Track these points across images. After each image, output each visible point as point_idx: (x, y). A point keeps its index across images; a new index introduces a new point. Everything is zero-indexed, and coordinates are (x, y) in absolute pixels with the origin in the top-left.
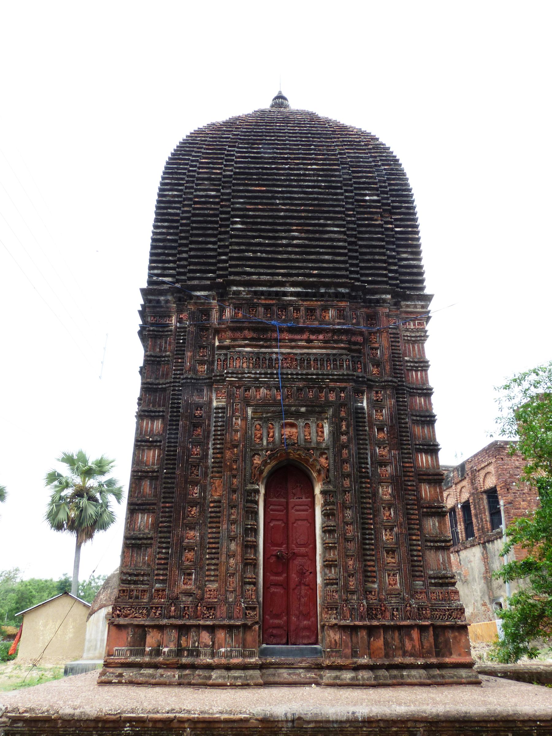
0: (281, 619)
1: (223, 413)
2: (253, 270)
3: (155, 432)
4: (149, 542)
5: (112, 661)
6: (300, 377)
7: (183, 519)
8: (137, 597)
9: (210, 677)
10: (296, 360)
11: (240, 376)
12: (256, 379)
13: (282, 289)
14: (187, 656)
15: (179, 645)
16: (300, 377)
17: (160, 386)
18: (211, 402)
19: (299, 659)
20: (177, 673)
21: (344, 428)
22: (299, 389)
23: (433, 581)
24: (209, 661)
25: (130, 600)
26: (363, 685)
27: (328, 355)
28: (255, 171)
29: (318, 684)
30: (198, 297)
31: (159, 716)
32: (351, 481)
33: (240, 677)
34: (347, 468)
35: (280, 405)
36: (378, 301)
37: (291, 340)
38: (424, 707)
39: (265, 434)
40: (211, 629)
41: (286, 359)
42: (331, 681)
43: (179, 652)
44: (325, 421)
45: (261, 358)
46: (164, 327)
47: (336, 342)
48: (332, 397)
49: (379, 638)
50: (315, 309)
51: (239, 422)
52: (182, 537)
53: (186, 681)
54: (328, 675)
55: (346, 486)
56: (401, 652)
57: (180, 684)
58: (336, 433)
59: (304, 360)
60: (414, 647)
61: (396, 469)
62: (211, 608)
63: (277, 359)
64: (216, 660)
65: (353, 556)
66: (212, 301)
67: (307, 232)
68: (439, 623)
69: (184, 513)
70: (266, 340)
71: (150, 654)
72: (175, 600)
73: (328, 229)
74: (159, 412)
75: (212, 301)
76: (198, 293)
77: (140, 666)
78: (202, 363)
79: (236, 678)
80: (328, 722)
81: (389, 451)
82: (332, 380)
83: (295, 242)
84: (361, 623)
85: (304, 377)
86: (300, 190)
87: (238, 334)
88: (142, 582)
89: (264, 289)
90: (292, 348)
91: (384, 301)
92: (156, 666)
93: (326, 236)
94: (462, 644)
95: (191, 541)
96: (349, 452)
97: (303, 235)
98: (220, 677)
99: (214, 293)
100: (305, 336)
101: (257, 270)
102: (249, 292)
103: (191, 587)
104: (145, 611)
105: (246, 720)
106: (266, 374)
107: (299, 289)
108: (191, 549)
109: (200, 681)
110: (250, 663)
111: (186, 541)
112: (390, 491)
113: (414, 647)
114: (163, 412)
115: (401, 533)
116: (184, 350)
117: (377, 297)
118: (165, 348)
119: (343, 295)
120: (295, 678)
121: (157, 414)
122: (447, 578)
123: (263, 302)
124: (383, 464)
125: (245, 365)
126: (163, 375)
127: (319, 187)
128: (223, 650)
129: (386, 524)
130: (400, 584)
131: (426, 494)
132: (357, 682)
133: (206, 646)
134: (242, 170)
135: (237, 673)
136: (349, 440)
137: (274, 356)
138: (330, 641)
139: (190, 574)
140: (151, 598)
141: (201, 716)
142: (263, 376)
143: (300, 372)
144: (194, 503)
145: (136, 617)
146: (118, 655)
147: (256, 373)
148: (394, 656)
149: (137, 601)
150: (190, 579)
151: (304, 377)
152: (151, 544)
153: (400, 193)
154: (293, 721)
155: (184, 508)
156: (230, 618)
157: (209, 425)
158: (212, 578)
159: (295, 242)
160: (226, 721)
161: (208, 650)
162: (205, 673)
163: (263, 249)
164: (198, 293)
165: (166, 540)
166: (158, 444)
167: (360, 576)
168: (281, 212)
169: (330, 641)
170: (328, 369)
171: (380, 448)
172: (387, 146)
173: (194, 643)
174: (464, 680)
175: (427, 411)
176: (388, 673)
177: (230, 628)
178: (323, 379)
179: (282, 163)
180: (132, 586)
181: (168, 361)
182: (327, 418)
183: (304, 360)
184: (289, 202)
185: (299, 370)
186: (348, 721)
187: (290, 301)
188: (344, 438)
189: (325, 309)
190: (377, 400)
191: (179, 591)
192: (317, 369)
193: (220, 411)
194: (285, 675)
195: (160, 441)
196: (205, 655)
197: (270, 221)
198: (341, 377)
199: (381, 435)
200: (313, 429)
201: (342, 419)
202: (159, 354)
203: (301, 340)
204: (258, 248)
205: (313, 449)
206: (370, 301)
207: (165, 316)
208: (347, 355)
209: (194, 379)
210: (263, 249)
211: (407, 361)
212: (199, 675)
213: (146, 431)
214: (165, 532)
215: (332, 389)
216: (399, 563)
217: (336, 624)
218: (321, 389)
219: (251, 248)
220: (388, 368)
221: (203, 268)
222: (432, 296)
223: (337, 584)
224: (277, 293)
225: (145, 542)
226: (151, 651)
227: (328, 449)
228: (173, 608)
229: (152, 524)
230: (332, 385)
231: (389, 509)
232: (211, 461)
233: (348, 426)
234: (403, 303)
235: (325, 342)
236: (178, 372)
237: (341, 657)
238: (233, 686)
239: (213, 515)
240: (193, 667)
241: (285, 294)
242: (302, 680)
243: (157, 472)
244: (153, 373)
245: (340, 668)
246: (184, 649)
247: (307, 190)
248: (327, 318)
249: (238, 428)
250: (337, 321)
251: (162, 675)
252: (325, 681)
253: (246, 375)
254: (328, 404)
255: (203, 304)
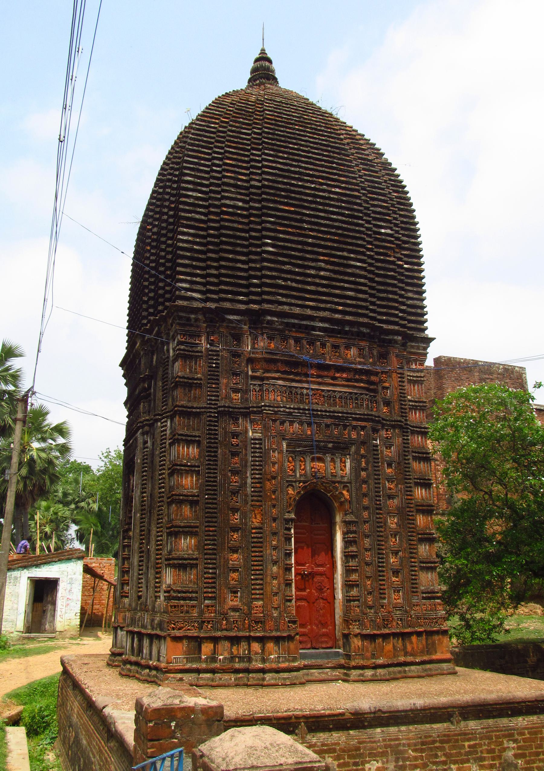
0: (306, 628)
1: (260, 444)
2: (284, 300)
3: (192, 456)
4: (195, 562)
5: (172, 668)
6: (328, 414)
7: (228, 543)
8: (187, 612)
9: (264, 679)
10: (324, 396)
11: (276, 409)
12: (290, 414)
13: (312, 323)
14: (239, 662)
15: (232, 653)
16: (328, 414)
17: (194, 410)
18: (246, 431)
19: (326, 661)
20: (233, 677)
21: (363, 464)
22: (327, 426)
23: (424, 595)
24: (261, 666)
25: (182, 615)
26: (381, 680)
27: (351, 393)
28: (283, 187)
29: (344, 681)
30: (231, 321)
31: (279, 714)
32: (369, 513)
33: (288, 678)
34: (366, 502)
35: (312, 440)
36: (390, 341)
37: (318, 376)
38: (457, 697)
39: (298, 467)
40: (261, 640)
41: (315, 395)
42: (357, 678)
43: (232, 659)
44: (348, 457)
45: (294, 392)
46: (192, 347)
47: (357, 381)
48: (354, 435)
49: (389, 643)
50: (338, 346)
51: (276, 454)
52: (228, 559)
53: (242, 683)
54: (355, 673)
55: (365, 517)
56: (403, 653)
57: (237, 685)
58: (357, 469)
59: (330, 397)
60: (413, 648)
61: (402, 501)
62: (258, 622)
63: (307, 395)
64: (267, 665)
65: (371, 577)
66: (243, 326)
67: (332, 264)
68: (429, 629)
69: (228, 538)
70: (297, 374)
71: (206, 661)
72: (225, 615)
73: (353, 263)
74: (195, 436)
75: (243, 326)
76: (231, 317)
77: (198, 671)
78: (236, 391)
79: (285, 679)
80: (398, 711)
81: (396, 486)
82: (355, 419)
83: (322, 273)
84: (378, 632)
85: (331, 414)
86: (326, 215)
87: (272, 367)
88: (191, 599)
89: (296, 321)
90: (319, 384)
91: (396, 342)
92: (213, 671)
93: (349, 271)
94: (444, 644)
95: (235, 563)
96: (368, 487)
97: (329, 267)
98: (273, 678)
99: (246, 318)
100: (331, 373)
101: (289, 300)
102: (282, 323)
103: (237, 603)
104: (196, 625)
105: (342, 714)
106: (299, 409)
107: (326, 325)
108: (235, 570)
109: (255, 682)
110: (295, 667)
111: (231, 562)
112: (396, 520)
113: (413, 648)
114: (199, 437)
115: (405, 557)
116: (218, 376)
117: (390, 337)
118: (195, 369)
119: (364, 335)
120: (324, 676)
121: (193, 439)
122: (434, 592)
123: (294, 334)
124: (391, 497)
125: (279, 398)
126: (195, 397)
127: (343, 215)
128: (272, 657)
129: (393, 549)
130: (403, 599)
131: (420, 522)
132: (376, 678)
133: (256, 653)
134: (271, 184)
135: (286, 675)
136: (368, 476)
137: (305, 391)
138: (355, 647)
139: (236, 592)
140: (201, 613)
141: (312, 713)
142: (296, 411)
143: (328, 410)
144: (235, 529)
145: (189, 630)
146: (177, 662)
147: (290, 408)
148: (398, 656)
149: (188, 615)
150: (235, 597)
151: (331, 414)
152: (197, 564)
153: (408, 226)
154: (374, 713)
155: (228, 533)
156: (277, 630)
157: (246, 455)
158: (258, 596)
159: (322, 273)
160: (330, 716)
161: (259, 657)
162: (260, 675)
163: (294, 277)
164: (231, 317)
165: (212, 561)
166: (197, 469)
167: (376, 593)
168: (309, 238)
169: (355, 647)
170: (351, 408)
171: (388, 482)
172: (393, 166)
173: (244, 651)
174: (445, 672)
175: (423, 447)
176: (396, 670)
177: (277, 640)
178: (348, 417)
179: (308, 181)
180: (182, 602)
181: (201, 384)
182: (349, 454)
183: (330, 397)
184: (317, 228)
185: (326, 407)
186: (411, 710)
187: (318, 335)
188: (363, 474)
189: (348, 348)
190: (387, 438)
191: (229, 607)
192: (342, 407)
193: (257, 442)
194: (316, 674)
195: (198, 467)
196: (256, 661)
197: (300, 247)
198: (362, 417)
199: (389, 471)
200: (338, 464)
201: (363, 456)
202: (191, 376)
203: (327, 377)
204: (289, 276)
205: (339, 482)
206: (384, 341)
207: (195, 335)
208: (367, 395)
209: (231, 408)
210: (294, 277)
211: (410, 401)
212: (253, 678)
213: (183, 455)
214: (210, 554)
215: (354, 428)
216: (403, 582)
217: (359, 633)
218: (345, 427)
219: (283, 275)
220: (397, 407)
221: (235, 289)
222: (433, 339)
223: (358, 600)
224: (307, 327)
225: (191, 562)
226: (207, 658)
227: (350, 483)
228: (224, 622)
229: (195, 545)
230: (354, 423)
231: (395, 537)
232: (249, 490)
233: (367, 463)
234: (409, 344)
235: (348, 380)
236: (213, 398)
237: (363, 659)
238: (284, 685)
239: (255, 540)
240: (247, 671)
241: (314, 328)
242: (330, 678)
243: (198, 496)
244: (185, 395)
245: (363, 667)
246: (235, 657)
247: (332, 216)
248: (349, 356)
249: (276, 460)
250: (358, 359)
251: (220, 679)
252: (352, 678)
253: (282, 409)
254: (352, 442)
255: (234, 328)
